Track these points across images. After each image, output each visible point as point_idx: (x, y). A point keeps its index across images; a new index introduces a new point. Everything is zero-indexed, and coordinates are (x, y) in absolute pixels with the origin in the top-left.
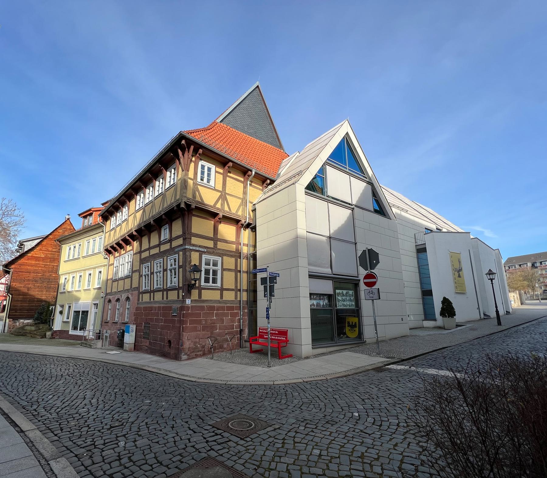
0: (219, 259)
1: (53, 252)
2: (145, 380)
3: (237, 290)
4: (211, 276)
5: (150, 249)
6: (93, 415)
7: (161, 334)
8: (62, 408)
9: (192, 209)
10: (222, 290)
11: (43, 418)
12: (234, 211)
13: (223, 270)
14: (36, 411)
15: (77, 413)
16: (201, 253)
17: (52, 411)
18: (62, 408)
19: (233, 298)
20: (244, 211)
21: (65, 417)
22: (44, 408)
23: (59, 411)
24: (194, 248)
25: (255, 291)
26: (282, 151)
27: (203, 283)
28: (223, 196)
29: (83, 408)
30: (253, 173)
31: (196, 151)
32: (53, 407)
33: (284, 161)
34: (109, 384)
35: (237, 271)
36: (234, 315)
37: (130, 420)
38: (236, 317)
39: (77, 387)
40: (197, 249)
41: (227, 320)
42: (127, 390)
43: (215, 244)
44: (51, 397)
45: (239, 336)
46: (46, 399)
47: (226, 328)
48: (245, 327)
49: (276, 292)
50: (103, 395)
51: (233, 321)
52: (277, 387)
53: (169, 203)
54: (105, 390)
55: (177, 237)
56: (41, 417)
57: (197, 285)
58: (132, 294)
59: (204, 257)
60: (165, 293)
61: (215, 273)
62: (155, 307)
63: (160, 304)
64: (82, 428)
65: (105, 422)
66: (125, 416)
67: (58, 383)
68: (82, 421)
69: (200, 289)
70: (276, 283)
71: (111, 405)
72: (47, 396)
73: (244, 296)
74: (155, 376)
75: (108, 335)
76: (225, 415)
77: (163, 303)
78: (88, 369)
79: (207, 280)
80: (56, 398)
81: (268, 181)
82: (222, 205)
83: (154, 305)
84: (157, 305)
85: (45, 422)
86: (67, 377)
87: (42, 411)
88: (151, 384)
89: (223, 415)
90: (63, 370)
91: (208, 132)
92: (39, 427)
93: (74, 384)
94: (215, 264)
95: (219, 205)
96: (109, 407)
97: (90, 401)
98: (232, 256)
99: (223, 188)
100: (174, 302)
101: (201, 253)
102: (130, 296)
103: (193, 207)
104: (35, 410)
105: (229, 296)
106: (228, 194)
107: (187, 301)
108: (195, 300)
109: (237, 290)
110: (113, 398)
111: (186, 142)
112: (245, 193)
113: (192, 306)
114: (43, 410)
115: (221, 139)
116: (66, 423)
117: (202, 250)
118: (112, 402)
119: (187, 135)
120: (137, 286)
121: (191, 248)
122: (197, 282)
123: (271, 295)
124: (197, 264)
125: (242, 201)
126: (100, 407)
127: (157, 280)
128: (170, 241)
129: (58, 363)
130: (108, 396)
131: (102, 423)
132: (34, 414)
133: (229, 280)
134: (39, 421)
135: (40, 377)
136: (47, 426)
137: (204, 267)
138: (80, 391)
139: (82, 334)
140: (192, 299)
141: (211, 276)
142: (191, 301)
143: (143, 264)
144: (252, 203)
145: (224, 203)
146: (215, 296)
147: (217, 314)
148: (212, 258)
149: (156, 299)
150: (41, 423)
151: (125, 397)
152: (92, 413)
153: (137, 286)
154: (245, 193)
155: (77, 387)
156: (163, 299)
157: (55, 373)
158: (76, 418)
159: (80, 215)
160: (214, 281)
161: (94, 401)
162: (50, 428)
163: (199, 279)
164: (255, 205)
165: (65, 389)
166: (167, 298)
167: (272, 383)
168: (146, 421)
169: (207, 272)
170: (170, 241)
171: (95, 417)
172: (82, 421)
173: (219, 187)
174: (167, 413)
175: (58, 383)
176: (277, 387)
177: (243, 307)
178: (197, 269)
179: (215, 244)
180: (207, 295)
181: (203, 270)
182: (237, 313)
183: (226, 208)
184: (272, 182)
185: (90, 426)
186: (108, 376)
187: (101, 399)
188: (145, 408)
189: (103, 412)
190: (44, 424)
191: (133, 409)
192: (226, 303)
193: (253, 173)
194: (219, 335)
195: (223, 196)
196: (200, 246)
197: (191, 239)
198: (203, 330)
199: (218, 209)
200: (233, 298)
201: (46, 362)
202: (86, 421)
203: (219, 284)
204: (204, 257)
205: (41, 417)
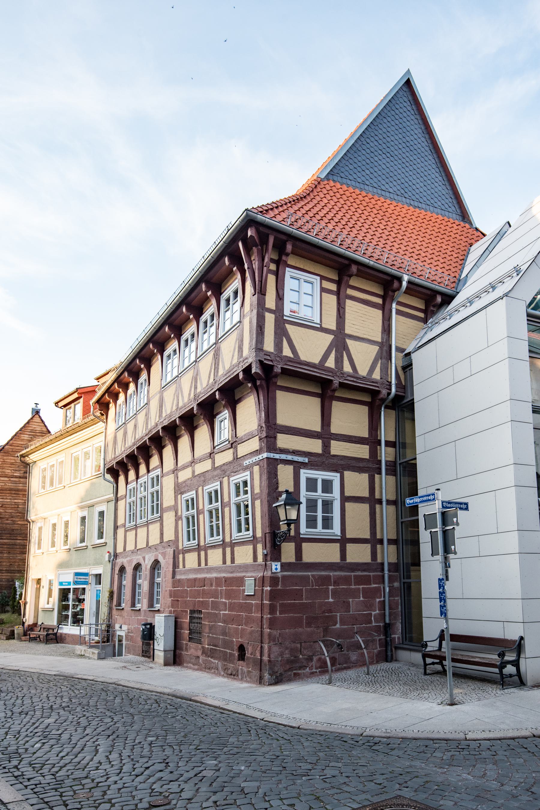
0: (335, 477)
1: (16, 477)
2: (200, 722)
3: (374, 541)
4: (320, 514)
5: (193, 462)
6: (116, 782)
7: (224, 633)
8: (61, 767)
9: (276, 376)
10: (344, 541)
11: (32, 782)
12: (363, 371)
13: (345, 499)
14: (18, 769)
15: (86, 777)
16: (298, 466)
17: (45, 771)
18: (61, 767)
19: (367, 559)
20: (385, 370)
21: (68, 782)
22: (30, 765)
23: (57, 772)
24: (283, 457)
25: (416, 543)
26: (467, 226)
27: (303, 529)
28: (340, 341)
29: (97, 768)
30: (404, 284)
31: (280, 248)
32: (44, 765)
33: (472, 248)
34: (136, 727)
35: (373, 501)
36: (370, 594)
37: (184, 795)
38: (375, 598)
39: (80, 730)
40: (290, 457)
41: (355, 603)
42: (170, 738)
43: (326, 447)
44: (38, 745)
45: (382, 637)
46: (31, 750)
47: (355, 620)
48: (395, 618)
49: (460, 545)
50: (128, 748)
51: (369, 606)
52: (473, 745)
53: (227, 367)
54: (131, 736)
55: (249, 437)
56: (29, 780)
57: (292, 533)
58: (164, 555)
59: (304, 474)
60: (228, 550)
61: (327, 505)
62: (211, 579)
63: (220, 572)
64: (100, 804)
65: (140, 797)
66: (174, 787)
67: (47, 721)
68: (97, 793)
69: (299, 542)
70: (458, 524)
71: (147, 765)
72: (31, 743)
73: (389, 555)
74: (219, 715)
75: (123, 634)
76: (368, 797)
77: (224, 572)
78: (95, 699)
79: (311, 522)
80: (46, 747)
81: (439, 299)
82: (339, 361)
83: (208, 576)
84: (214, 575)
85: (36, 790)
86: (62, 712)
87: (29, 773)
88: (212, 729)
89: (364, 796)
90: (52, 699)
91: (302, 203)
92: (27, 797)
93: (75, 723)
94: (327, 486)
95: (331, 363)
96: (142, 769)
97: (107, 757)
98: (360, 470)
99: (337, 324)
100: (245, 568)
101: (298, 466)
102: (160, 559)
103: (277, 370)
104: (16, 767)
105: (359, 554)
106: (351, 337)
107: (274, 567)
108: (290, 564)
109: (374, 541)
110: (146, 752)
111: (258, 232)
112: (387, 329)
113: (284, 577)
114: (30, 769)
115: (324, 212)
116: (71, 793)
117: (300, 459)
118: (145, 760)
119: (260, 217)
120: (173, 538)
121: (277, 456)
122: (292, 526)
123: (447, 550)
124: (291, 490)
125: (381, 348)
126: (125, 769)
127: (141, 511)
128: (233, 444)
129: (41, 685)
130: (137, 749)
131: (133, 797)
132: (16, 774)
133: (358, 521)
134: (26, 787)
135: (16, 710)
136: (41, 796)
137: (304, 495)
138: (87, 738)
139: (77, 633)
140: (283, 560)
141: (320, 514)
142: (282, 566)
143: (182, 493)
144: (402, 350)
145: (342, 357)
146: (330, 554)
147: (334, 592)
148: (320, 475)
149: (211, 563)
150: (29, 791)
151: (168, 751)
152: (113, 778)
153: (173, 538)
154: (387, 329)
155: (80, 730)
156: (224, 562)
157: (41, 705)
158: (86, 786)
159: (57, 404)
160: (327, 523)
161: (114, 756)
162: (46, 800)
163: (297, 522)
164: (409, 354)
165: (59, 732)
166: (233, 561)
167: (462, 736)
168: (214, 798)
169: (312, 505)
170: (233, 444)
171: (120, 785)
172: (97, 793)
173: (331, 323)
174: (250, 786)
175: (47, 721)
176: (473, 745)
177: (390, 577)
178: (293, 500)
179: (326, 447)
180: (312, 553)
181: (303, 500)
182: (378, 589)
183: (347, 368)
184: (448, 299)
185: (113, 801)
186: (132, 711)
187: (126, 753)
188: (208, 773)
189: (133, 777)
190: (35, 793)
191: (186, 775)
192: (353, 570)
193: (404, 284)
194: (339, 635)
195: (340, 341)
196: (295, 452)
197: (275, 438)
198: (309, 624)
199: (329, 370)
200: (367, 559)
201: (22, 683)
202: (105, 793)
203: (337, 530)
204: (304, 474)
205: (29, 780)
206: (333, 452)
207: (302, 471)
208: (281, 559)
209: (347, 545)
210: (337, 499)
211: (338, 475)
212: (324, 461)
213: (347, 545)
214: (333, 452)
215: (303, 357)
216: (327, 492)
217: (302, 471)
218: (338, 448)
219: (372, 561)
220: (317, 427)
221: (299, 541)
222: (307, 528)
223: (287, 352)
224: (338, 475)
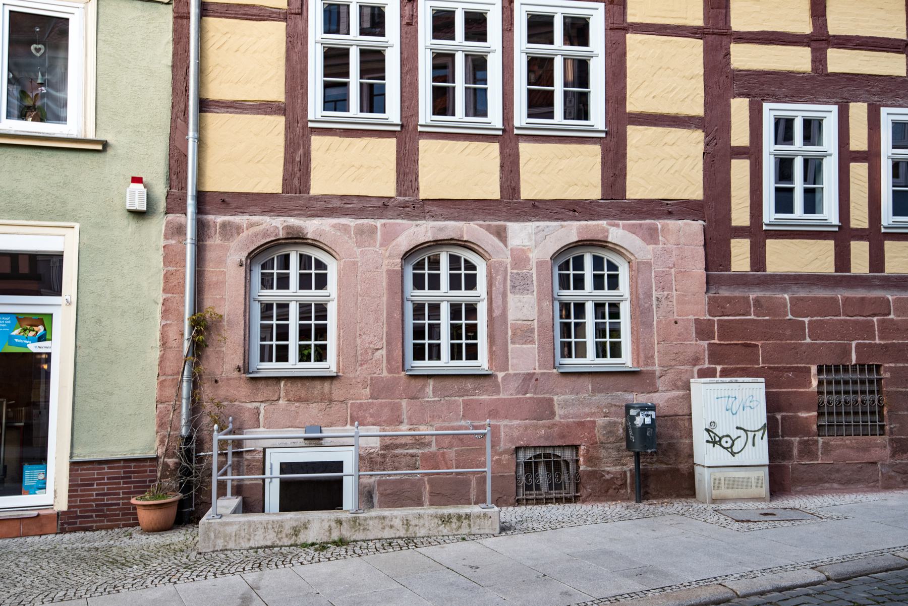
0: (829, 115)
10: (842, 236)
61: (813, 168)
94: (812, 130)
146: (818, 258)
148: (799, 111)
160: (812, 202)
179: (819, 61)
180: (783, 257)
204: (770, 111)
207: (766, 106)
208: (730, 264)
209: (732, 241)
210: (831, 155)
212: (819, 84)
213: (732, 241)
216: (444, 113)
217: (766, 106)
218: (840, 61)
219: (752, 270)
220: (805, 27)
221: (758, 234)
222: (777, 211)
224: (835, 108)
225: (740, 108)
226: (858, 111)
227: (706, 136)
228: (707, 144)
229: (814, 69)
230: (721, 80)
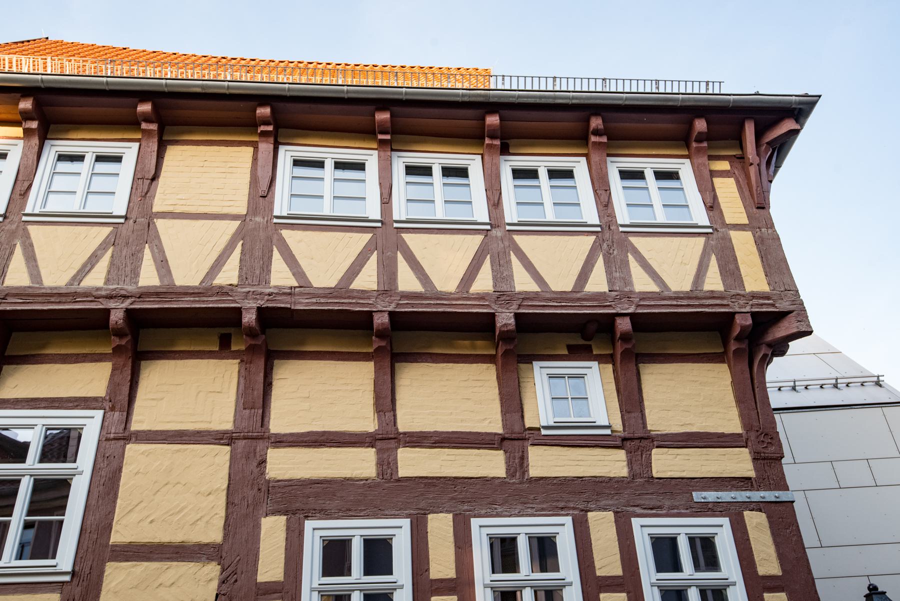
179: (518, 464)
204: (482, 530)
206: (534, 472)
211: (725, 521)
214: (534, 472)
215: (554, 288)
218: (543, 463)
223: (407, 281)
224: (406, 523)
225: (273, 529)
226: (440, 526)
227: (223, 570)
228: (223, 582)
229: (381, 473)
230: (251, 494)
